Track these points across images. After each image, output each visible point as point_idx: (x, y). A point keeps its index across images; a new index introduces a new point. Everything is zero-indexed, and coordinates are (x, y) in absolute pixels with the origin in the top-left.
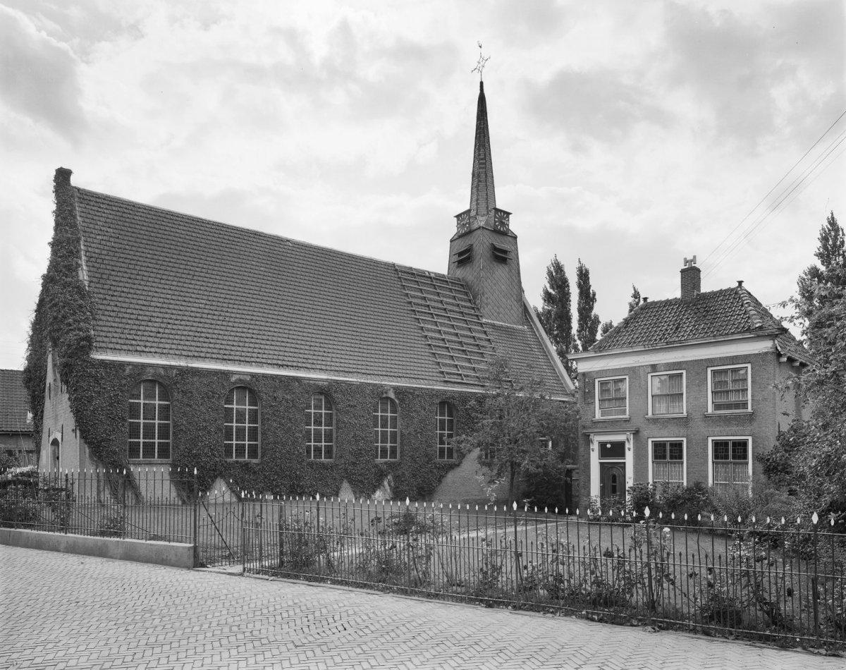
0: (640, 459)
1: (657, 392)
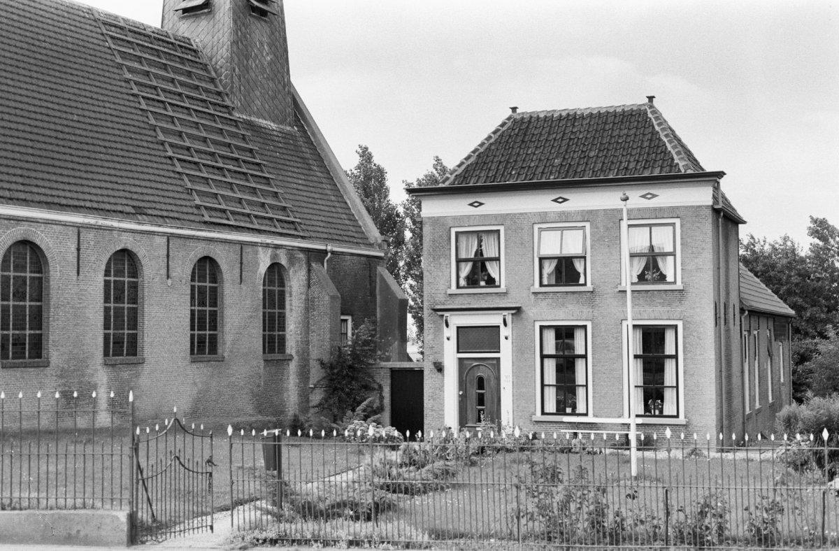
0: (522, 354)
1: (670, 259)
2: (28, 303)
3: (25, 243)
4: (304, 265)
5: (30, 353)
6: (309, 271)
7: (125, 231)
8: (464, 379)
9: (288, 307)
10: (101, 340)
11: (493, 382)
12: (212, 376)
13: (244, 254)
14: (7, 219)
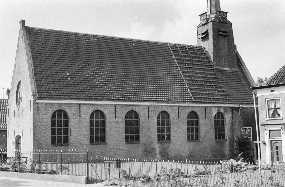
2: (194, 126)
3: (97, 111)
4: (231, 112)
5: (135, 140)
6: (233, 113)
7: (164, 106)
8: (272, 147)
9: (225, 125)
10: (157, 136)
11: (281, 148)
12: (196, 146)
13: (206, 110)
14: (126, 105)
